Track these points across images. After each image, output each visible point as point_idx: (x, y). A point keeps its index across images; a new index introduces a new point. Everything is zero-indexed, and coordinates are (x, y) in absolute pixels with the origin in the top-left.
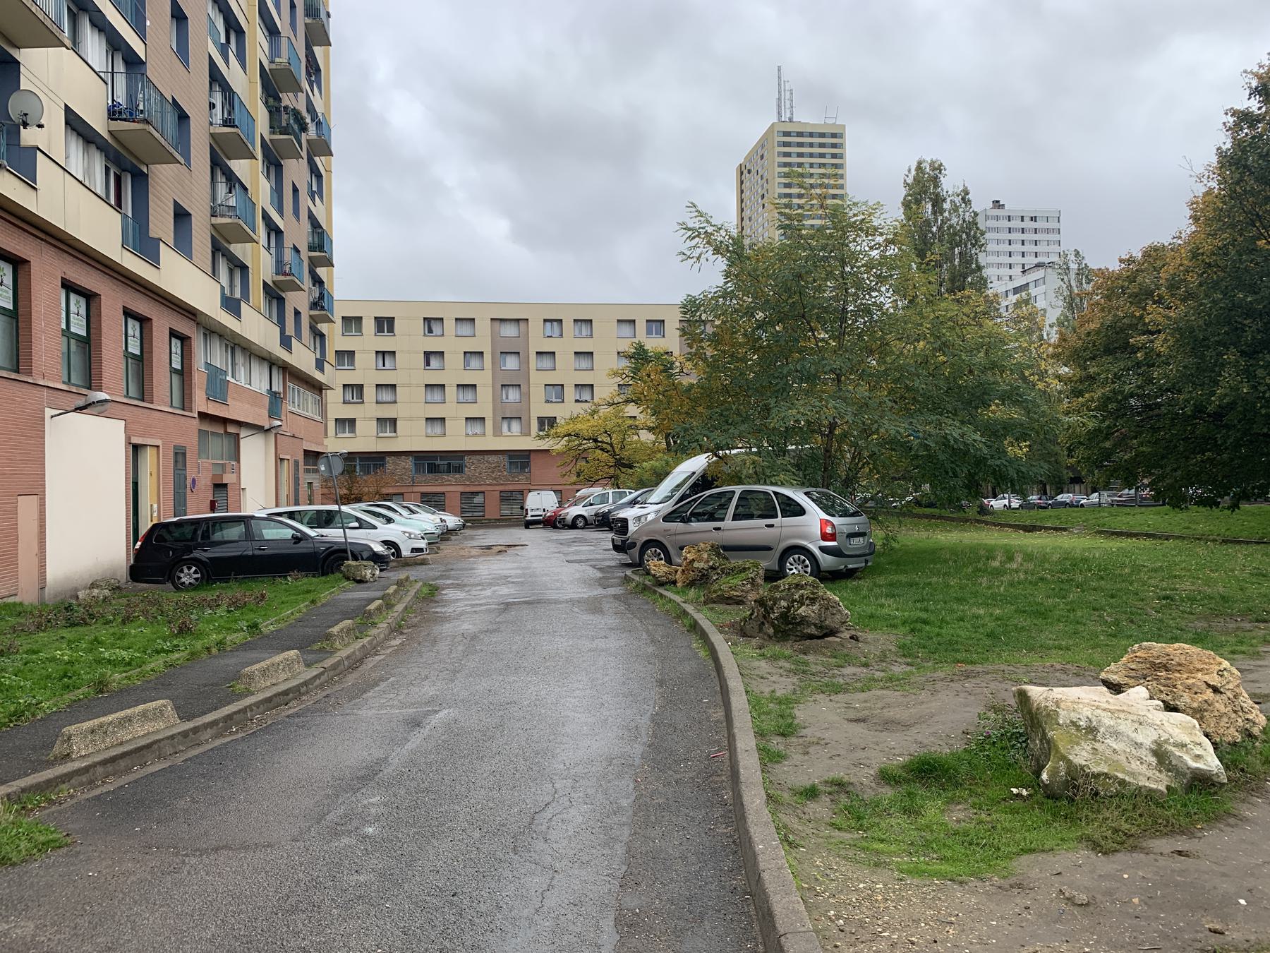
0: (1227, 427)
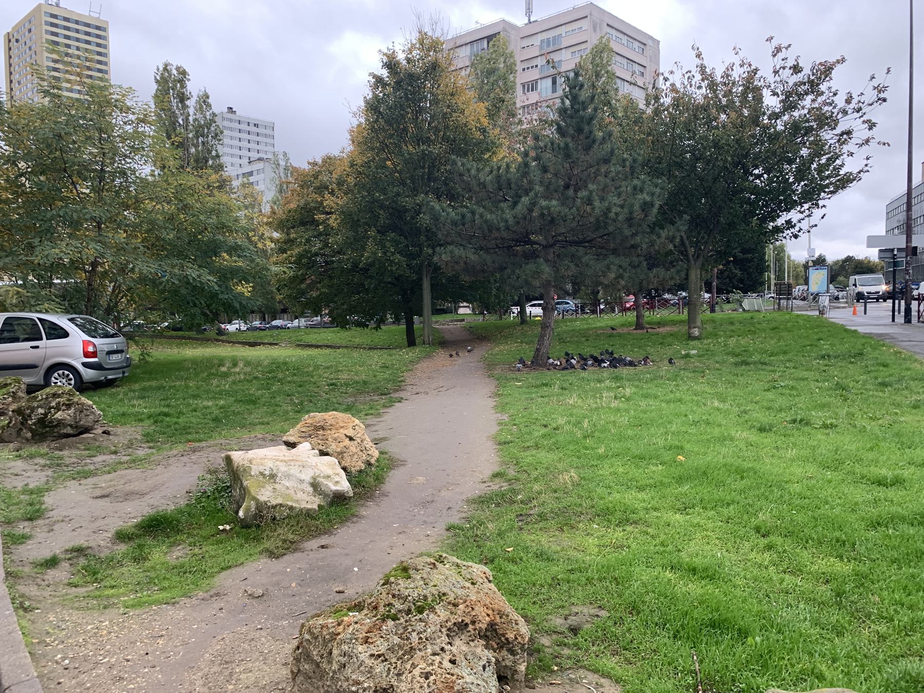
0: (371, 277)
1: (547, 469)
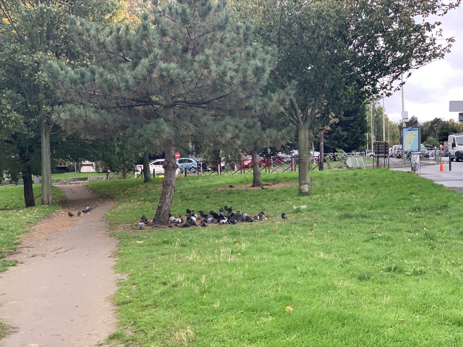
1: (164, 327)
